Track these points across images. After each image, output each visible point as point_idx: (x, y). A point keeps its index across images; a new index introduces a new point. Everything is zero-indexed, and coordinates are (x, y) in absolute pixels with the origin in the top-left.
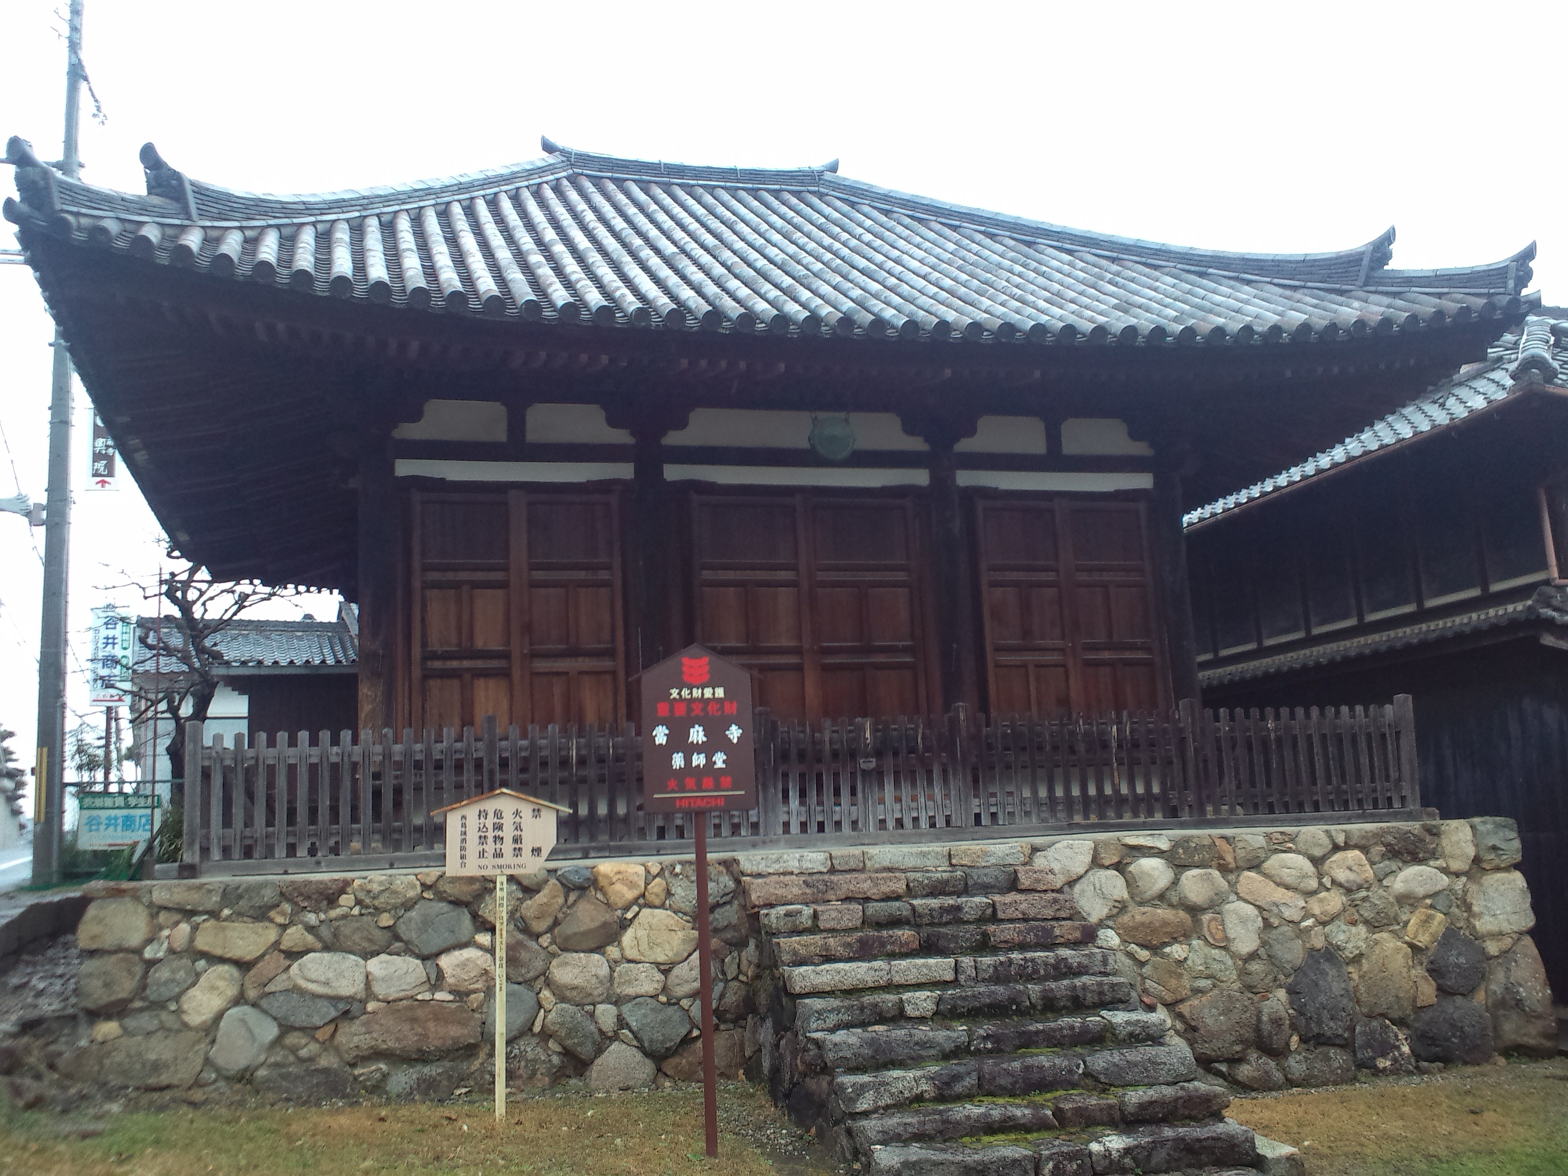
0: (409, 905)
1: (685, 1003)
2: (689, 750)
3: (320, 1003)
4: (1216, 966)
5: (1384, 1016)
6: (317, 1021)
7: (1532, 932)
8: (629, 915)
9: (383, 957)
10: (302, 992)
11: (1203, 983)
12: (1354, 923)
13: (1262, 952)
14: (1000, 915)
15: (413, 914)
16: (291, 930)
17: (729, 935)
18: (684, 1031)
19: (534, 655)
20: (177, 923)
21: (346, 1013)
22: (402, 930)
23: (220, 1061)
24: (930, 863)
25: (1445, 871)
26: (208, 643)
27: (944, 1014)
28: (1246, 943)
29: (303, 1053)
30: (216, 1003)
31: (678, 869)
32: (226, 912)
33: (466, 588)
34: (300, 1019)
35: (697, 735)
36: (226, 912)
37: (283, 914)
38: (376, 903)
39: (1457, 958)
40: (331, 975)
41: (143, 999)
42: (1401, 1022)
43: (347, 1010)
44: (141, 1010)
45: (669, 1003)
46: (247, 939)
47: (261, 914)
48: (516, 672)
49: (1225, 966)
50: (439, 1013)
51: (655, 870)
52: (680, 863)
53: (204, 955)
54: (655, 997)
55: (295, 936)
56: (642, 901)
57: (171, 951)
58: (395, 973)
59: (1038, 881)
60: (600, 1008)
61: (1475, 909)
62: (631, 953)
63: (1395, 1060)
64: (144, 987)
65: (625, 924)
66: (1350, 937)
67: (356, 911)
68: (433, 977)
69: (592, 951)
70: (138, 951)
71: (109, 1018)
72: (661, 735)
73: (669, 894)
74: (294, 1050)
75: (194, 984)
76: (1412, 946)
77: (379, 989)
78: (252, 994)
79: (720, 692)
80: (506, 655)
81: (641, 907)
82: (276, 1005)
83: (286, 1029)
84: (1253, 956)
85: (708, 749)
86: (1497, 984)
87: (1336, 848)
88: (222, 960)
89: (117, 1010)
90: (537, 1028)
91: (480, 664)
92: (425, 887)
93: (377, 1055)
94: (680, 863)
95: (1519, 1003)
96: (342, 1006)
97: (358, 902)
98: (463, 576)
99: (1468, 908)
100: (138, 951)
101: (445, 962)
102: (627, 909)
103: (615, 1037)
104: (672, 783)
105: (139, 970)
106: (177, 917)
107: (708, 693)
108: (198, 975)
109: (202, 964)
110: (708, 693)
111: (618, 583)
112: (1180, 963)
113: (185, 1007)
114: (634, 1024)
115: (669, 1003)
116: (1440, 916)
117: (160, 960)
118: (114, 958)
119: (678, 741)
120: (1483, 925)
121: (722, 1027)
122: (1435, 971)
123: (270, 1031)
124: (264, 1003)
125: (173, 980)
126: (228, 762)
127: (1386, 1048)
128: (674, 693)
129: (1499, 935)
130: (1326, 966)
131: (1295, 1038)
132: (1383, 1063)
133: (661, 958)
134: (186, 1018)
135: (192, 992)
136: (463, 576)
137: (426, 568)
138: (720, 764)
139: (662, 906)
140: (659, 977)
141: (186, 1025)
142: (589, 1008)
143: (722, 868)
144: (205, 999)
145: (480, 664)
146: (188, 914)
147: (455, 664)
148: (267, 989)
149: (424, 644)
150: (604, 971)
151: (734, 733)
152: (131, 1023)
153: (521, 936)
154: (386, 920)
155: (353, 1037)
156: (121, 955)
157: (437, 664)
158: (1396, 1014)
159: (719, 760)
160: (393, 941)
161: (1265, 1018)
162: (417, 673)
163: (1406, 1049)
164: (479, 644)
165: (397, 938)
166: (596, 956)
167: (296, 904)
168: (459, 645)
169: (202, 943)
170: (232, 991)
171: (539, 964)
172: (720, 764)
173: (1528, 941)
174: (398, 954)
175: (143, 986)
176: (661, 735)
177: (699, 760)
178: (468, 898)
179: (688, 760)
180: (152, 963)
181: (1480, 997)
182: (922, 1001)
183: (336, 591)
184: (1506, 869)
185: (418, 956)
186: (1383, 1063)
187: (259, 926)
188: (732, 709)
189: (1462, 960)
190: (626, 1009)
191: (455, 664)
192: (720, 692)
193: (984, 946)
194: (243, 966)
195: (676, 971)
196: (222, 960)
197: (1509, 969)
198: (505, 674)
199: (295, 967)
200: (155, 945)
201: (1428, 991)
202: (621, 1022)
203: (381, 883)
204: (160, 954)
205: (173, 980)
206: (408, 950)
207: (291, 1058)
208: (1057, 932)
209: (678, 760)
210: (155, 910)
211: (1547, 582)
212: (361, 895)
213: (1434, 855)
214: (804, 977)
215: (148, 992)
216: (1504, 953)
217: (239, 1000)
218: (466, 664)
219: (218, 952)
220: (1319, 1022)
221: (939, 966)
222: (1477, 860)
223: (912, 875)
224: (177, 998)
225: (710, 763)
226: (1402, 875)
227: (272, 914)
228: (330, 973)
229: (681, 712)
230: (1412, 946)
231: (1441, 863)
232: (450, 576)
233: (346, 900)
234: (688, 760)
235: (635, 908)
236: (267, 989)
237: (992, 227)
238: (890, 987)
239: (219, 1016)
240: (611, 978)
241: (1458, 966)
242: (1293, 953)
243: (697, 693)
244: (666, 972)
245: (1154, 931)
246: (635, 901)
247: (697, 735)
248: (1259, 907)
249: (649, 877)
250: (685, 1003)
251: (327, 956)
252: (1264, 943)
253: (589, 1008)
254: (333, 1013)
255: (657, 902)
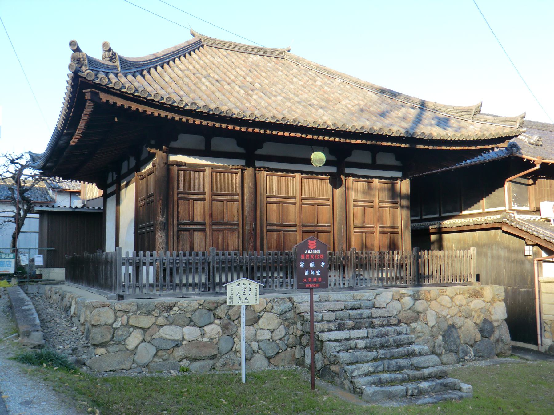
0: (195, 311)
1: (278, 342)
2: (310, 269)
3: (170, 342)
4: (424, 329)
5: (467, 344)
6: (168, 347)
7: (506, 320)
8: (261, 314)
9: (188, 327)
10: (164, 339)
11: (420, 334)
12: (461, 316)
13: (436, 325)
14: (373, 316)
15: (196, 313)
16: (160, 318)
17: (290, 321)
18: (277, 350)
19: (213, 224)
20: (123, 316)
21: (177, 345)
22: (193, 318)
23: (138, 361)
24: (348, 299)
25: (484, 301)
26: (25, 195)
27: (368, 348)
28: (432, 323)
29: (164, 358)
30: (137, 342)
31: (276, 300)
32: (139, 312)
33: (191, 201)
34: (163, 347)
35: (312, 265)
36: (139, 312)
37: (157, 313)
38: (185, 310)
39: (487, 327)
40: (172, 333)
41: (113, 341)
42: (471, 346)
43: (178, 345)
44: (112, 344)
45: (273, 342)
46: (145, 321)
47: (149, 313)
48: (207, 230)
49: (427, 330)
50: (205, 344)
51: (269, 301)
52: (277, 298)
53: (132, 326)
54: (269, 340)
55: (161, 320)
56: (265, 310)
57: (122, 325)
58: (190, 333)
59: (380, 305)
60: (253, 343)
61: (492, 313)
62: (261, 327)
63: (470, 357)
64: (113, 337)
65: (259, 317)
66: (459, 321)
67: (178, 312)
68: (203, 333)
69: (250, 325)
70: (111, 325)
71: (103, 347)
72: (302, 265)
73: (273, 308)
74: (161, 357)
75: (129, 336)
76: (475, 323)
77: (186, 337)
78: (148, 338)
79: (319, 252)
80: (204, 224)
81: (265, 312)
82: (156, 342)
83: (158, 350)
84: (433, 326)
85: (315, 269)
86: (496, 334)
87: (457, 294)
88: (138, 328)
89: (103, 345)
90: (234, 350)
91: (196, 227)
92: (200, 305)
93: (187, 358)
94: (277, 298)
95: (502, 341)
96: (176, 343)
97: (179, 309)
98: (191, 196)
99: (490, 312)
100: (111, 325)
101: (206, 328)
102: (260, 312)
103: (257, 352)
104: (305, 280)
105: (112, 331)
106: (123, 314)
107: (315, 252)
108: (131, 333)
109: (131, 329)
110: (315, 252)
111: (240, 201)
112: (415, 328)
113: (127, 343)
114: (263, 348)
115: (273, 342)
116: (483, 315)
117: (118, 328)
118: (104, 327)
119: (307, 267)
120: (493, 318)
121: (288, 349)
122: (481, 331)
123: (154, 351)
124: (152, 342)
125: (123, 335)
126: (130, 261)
127: (466, 353)
128: (306, 251)
129: (497, 321)
130: (453, 329)
131: (444, 350)
132: (467, 358)
133: (271, 328)
134: (127, 347)
135: (129, 338)
136: (191, 196)
137: (179, 193)
138: (318, 274)
139: (271, 312)
140: (270, 334)
141: (127, 349)
142: (250, 343)
143: (288, 300)
144: (134, 340)
145: (196, 227)
146: (126, 312)
147: (188, 227)
148: (153, 337)
149: (178, 219)
150: (254, 332)
151: (323, 264)
152: (110, 349)
153: (229, 321)
154: (189, 315)
155: (179, 353)
156: (106, 326)
157: (182, 226)
158: (470, 343)
159: (318, 272)
160: (191, 322)
161: (436, 344)
162: (176, 229)
163: (473, 354)
164: (195, 220)
165: (191, 321)
166: (252, 327)
167: (161, 310)
168: (189, 220)
169: (131, 323)
170: (141, 338)
171: (235, 330)
172: (318, 274)
173: (505, 322)
174: (192, 326)
175: (113, 337)
176: (302, 265)
177: (312, 272)
178: (213, 309)
179: (309, 272)
180: (115, 329)
181: (492, 338)
182: (361, 344)
183: (95, 184)
184: (500, 301)
185: (198, 327)
186: (467, 358)
187: (150, 317)
188: (322, 257)
189: (488, 328)
190: (261, 344)
191: (188, 227)
192: (319, 252)
193: (372, 326)
194: (144, 330)
195: (275, 332)
196: (138, 328)
197: (500, 330)
198: (204, 230)
199: (161, 330)
200: (116, 323)
201: (479, 337)
202: (260, 348)
203: (187, 304)
204: (119, 326)
205: (123, 335)
206: (195, 325)
207: (161, 360)
208: (391, 321)
209: (307, 273)
210: (115, 311)
211: (505, 211)
212: (181, 307)
213: (482, 296)
214: (325, 336)
215: (115, 338)
216: (498, 326)
217: (144, 341)
218: (191, 227)
219: (137, 325)
220: (451, 345)
221: (362, 333)
222: (493, 298)
223: (346, 303)
224: (124, 340)
225: (316, 273)
226: (473, 302)
227: (154, 313)
228: (170, 332)
229: (308, 257)
230: (475, 323)
231: (483, 299)
232: (186, 196)
233: (176, 309)
234: (309, 272)
235: (263, 312)
236: (153, 337)
237: (263, 52)
238: (350, 339)
239: (137, 346)
240: (256, 334)
241: (487, 329)
242: (445, 326)
243: (312, 252)
244: (272, 332)
245: (408, 319)
246: (263, 310)
247: (312, 265)
248: (436, 312)
249: (267, 303)
250: (278, 342)
251: (171, 327)
252: (437, 322)
253: (250, 343)
254: (174, 345)
255: (269, 310)
